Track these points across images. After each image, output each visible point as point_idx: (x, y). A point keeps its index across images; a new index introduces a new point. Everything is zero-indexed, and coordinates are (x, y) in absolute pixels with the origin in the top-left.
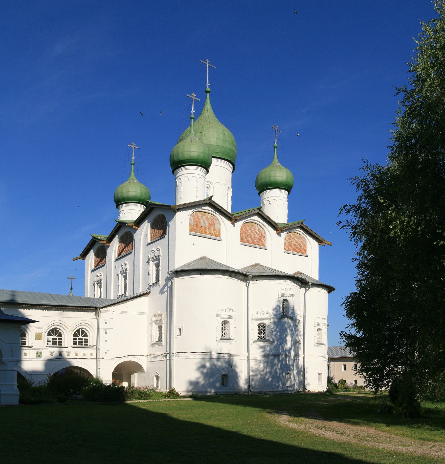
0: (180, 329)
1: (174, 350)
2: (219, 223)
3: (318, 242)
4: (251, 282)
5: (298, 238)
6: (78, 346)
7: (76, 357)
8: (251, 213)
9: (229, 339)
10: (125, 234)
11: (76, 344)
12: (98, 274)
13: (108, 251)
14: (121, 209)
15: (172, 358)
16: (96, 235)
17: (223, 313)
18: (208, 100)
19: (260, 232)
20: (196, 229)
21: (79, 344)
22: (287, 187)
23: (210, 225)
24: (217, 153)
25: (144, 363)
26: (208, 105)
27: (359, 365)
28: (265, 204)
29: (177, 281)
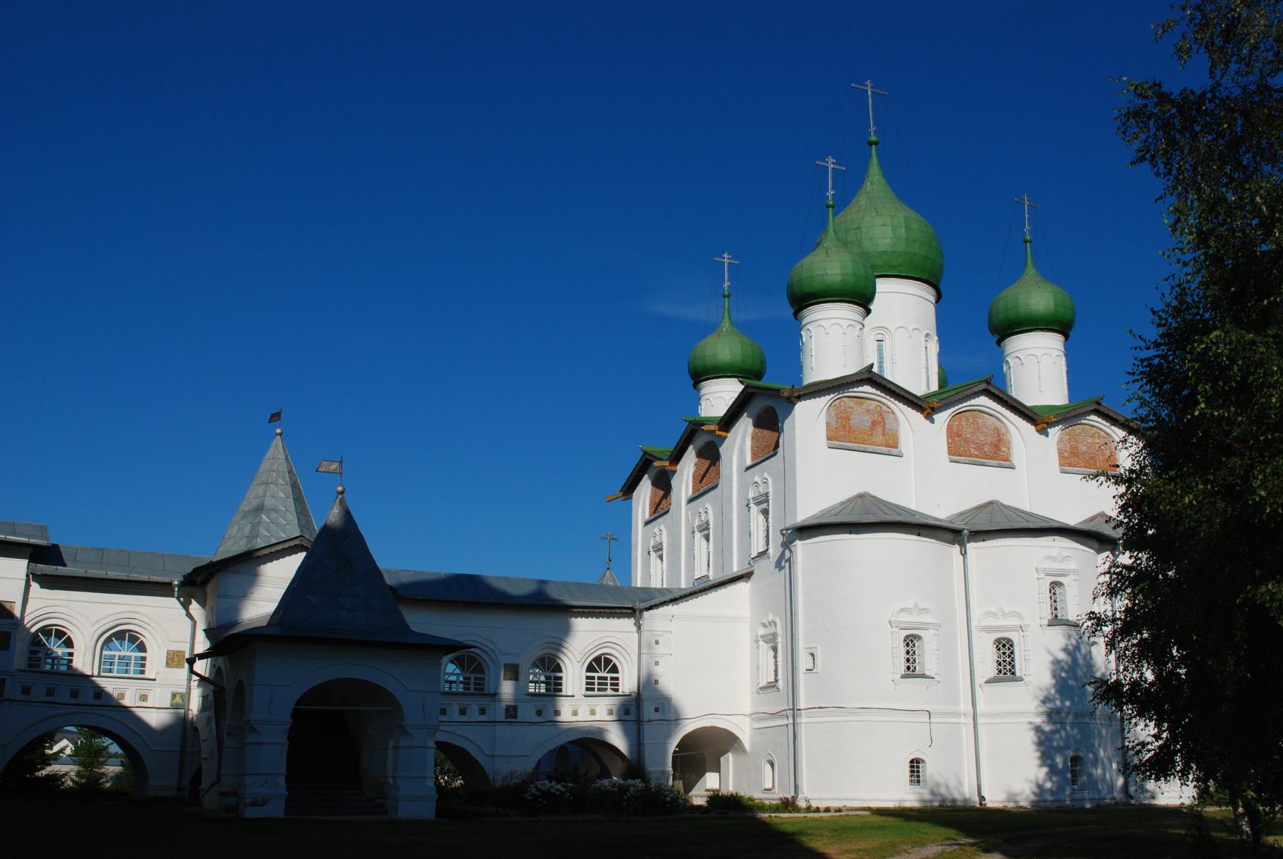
0: (812, 655)
1: (802, 704)
2: (896, 419)
5: (1093, 436)
6: (596, 692)
8: (968, 392)
9: (923, 676)
10: (705, 441)
11: (593, 689)
12: (656, 530)
13: (674, 482)
14: (703, 392)
15: (799, 720)
16: (649, 449)
17: (905, 618)
18: (874, 160)
19: (997, 430)
20: (842, 435)
21: (599, 690)
22: (1060, 325)
23: (874, 424)
24: (893, 267)
25: (744, 731)
26: (875, 171)
29: (801, 547)
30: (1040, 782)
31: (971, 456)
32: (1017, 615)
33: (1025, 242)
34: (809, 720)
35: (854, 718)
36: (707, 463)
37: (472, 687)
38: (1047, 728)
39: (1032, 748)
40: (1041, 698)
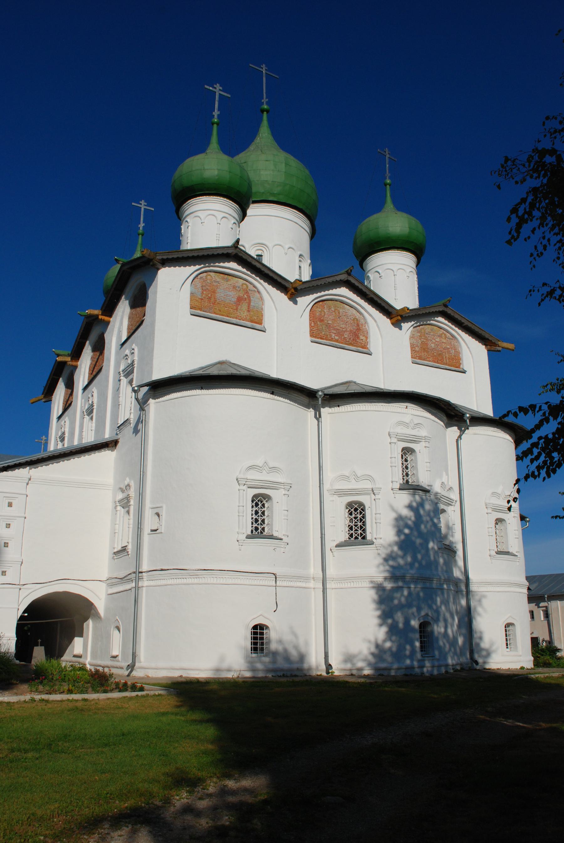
1: (144, 568)
2: (262, 298)
3: (486, 345)
4: (322, 410)
5: (440, 336)
8: (331, 280)
9: (271, 537)
17: (253, 475)
19: (356, 320)
20: (205, 305)
22: (415, 249)
23: (240, 300)
24: (273, 194)
27: (207, 223)
28: (372, 278)
30: (380, 642)
32: (369, 478)
33: (386, 185)
34: (152, 583)
35: (196, 581)
36: (98, 354)
38: (389, 585)
39: (373, 606)
40: (384, 556)
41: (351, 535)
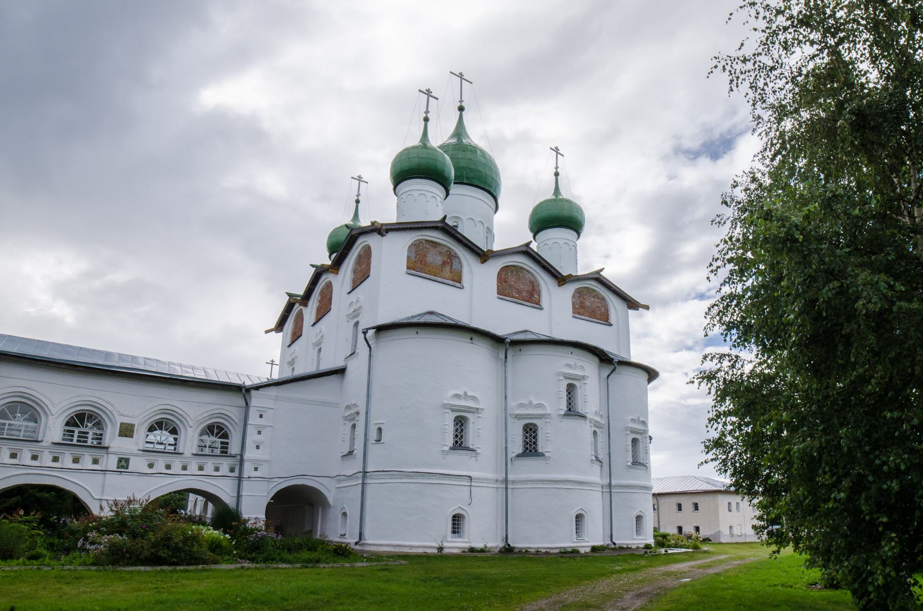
2: (460, 263)
7: (696, 499)
9: (468, 449)
19: (532, 282)
23: (444, 263)
31: (513, 297)
37: (75, 438)
41: (457, 442)
